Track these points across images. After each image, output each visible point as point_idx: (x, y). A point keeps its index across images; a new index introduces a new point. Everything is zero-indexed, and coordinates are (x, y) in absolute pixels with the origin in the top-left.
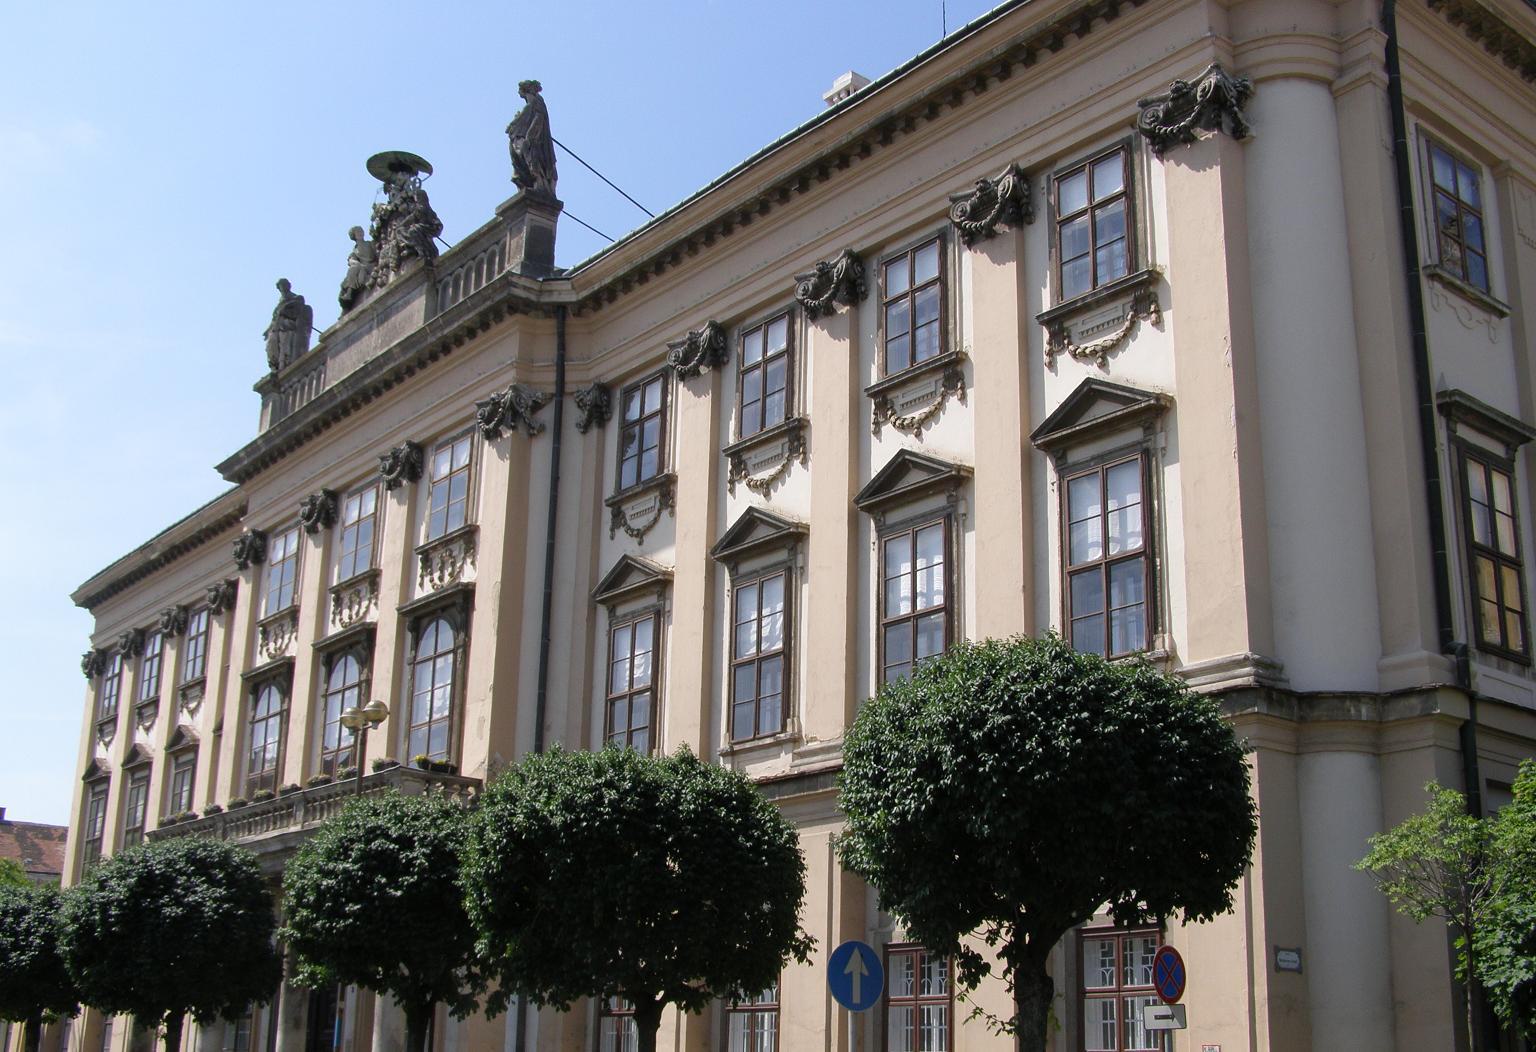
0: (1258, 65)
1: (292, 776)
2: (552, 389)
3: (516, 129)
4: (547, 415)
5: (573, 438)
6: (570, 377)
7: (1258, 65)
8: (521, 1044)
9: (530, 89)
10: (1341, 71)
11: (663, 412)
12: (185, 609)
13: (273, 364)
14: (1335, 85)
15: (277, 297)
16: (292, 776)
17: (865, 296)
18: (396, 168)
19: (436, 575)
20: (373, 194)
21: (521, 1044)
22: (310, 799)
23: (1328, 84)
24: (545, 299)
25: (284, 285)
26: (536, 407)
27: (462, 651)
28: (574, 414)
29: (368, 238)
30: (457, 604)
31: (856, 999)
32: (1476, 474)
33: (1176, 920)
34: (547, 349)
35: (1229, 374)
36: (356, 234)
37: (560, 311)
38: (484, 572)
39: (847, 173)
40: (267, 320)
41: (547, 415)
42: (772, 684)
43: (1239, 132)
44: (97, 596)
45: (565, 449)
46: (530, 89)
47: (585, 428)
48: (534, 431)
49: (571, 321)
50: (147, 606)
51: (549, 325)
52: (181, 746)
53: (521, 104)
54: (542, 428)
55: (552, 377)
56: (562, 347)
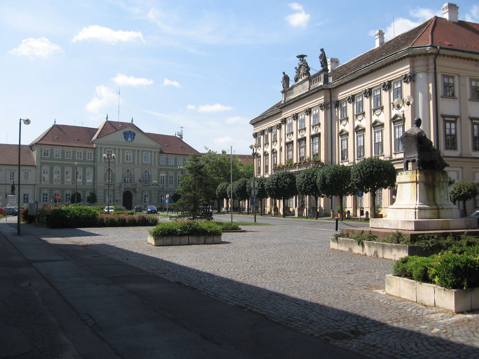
0: (416, 70)
1: (295, 161)
2: (330, 102)
3: (321, 57)
4: (329, 106)
5: (333, 108)
6: (332, 99)
7: (416, 70)
8: (478, 168)
9: (322, 50)
10: (428, 70)
11: (346, 106)
12: (272, 127)
13: (284, 87)
14: (427, 72)
15: (283, 75)
16: (295, 161)
17: (372, 96)
18: (302, 57)
19: (315, 130)
20: (298, 61)
21: (478, 168)
22: (300, 165)
23: (426, 72)
24: (327, 88)
25: (284, 73)
26: (327, 105)
27: (320, 142)
28: (333, 105)
29: (298, 68)
30: (318, 135)
31: (360, 196)
32: (448, 125)
33: (384, 189)
34: (328, 95)
35: (411, 116)
36: (296, 68)
37: (330, 89)
38: (321, 130)
39: (368, 76)
40: (282, 80)
41: (329, 106)
42: (362, 150)
43: (414, 81)
44: (255, 123)
45: (332, 111)
46: (322, 50)
47: (335, 108)
48: (327, 108)
49: (332, 90)
50: (265, 126)
51: (328, 91)
52: (274, 152)
53: (321, 53)
54: (329, 108)
55: (329, 99)
56: (331, 95)
